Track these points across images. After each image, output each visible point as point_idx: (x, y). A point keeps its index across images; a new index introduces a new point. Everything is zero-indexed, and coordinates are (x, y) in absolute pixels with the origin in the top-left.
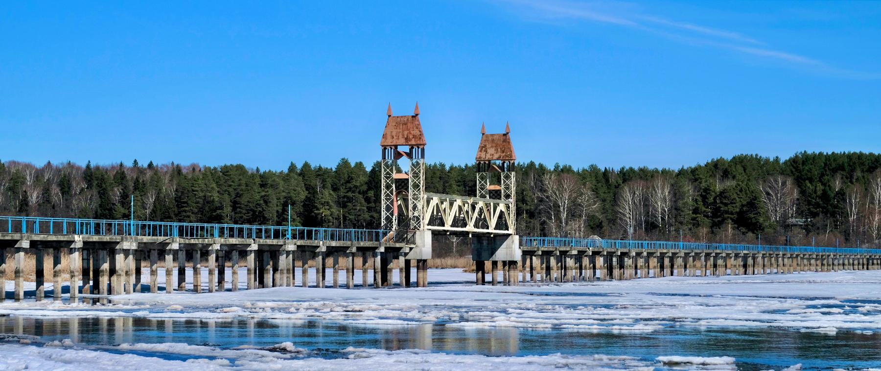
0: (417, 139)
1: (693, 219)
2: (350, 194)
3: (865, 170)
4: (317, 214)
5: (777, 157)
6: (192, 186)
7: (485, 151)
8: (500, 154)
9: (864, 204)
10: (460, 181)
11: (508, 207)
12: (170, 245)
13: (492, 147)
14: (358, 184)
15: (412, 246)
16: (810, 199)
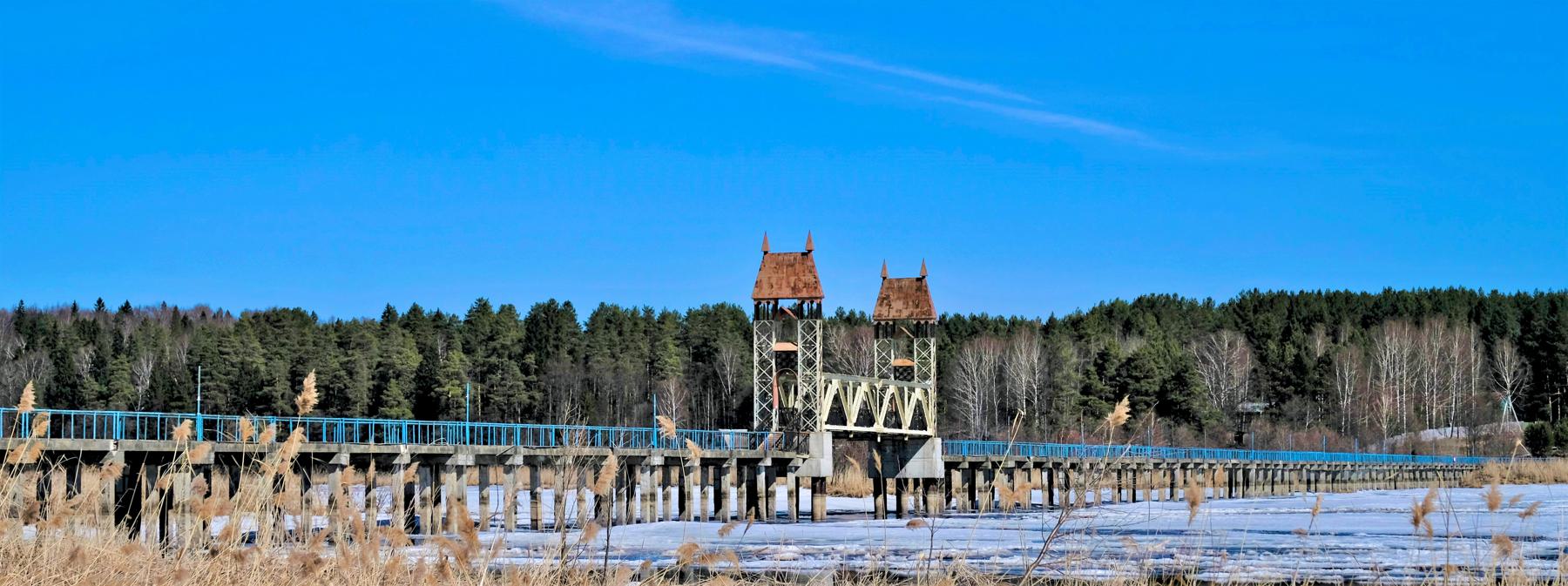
0: (810, 290)
1: (1084, 403)
2: (494, 359)
3: (1357, 321)
4: (441, 394)
5: (1209, 299)
6: (219, 346)
7: (887, 305)
8: (912, 309)
9: (1363, 380)
10: (679, 339)
11: (926, 393)
12: (511, 458)
13: (899, 298)
14: (509, 343)
15: (805, 456)
16: (1275, 371)
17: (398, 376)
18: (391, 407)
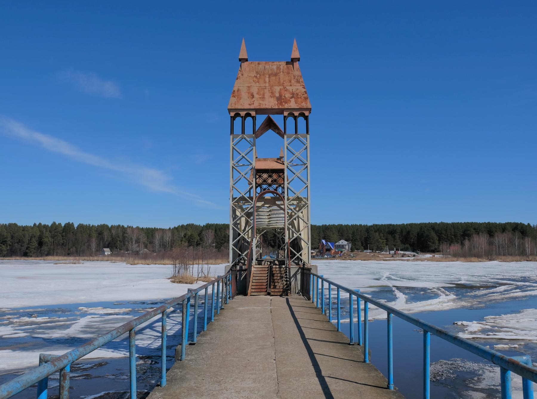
0: (299, 100)
2: (56, 234)
17: (34, 237)
18: (33, 243)
